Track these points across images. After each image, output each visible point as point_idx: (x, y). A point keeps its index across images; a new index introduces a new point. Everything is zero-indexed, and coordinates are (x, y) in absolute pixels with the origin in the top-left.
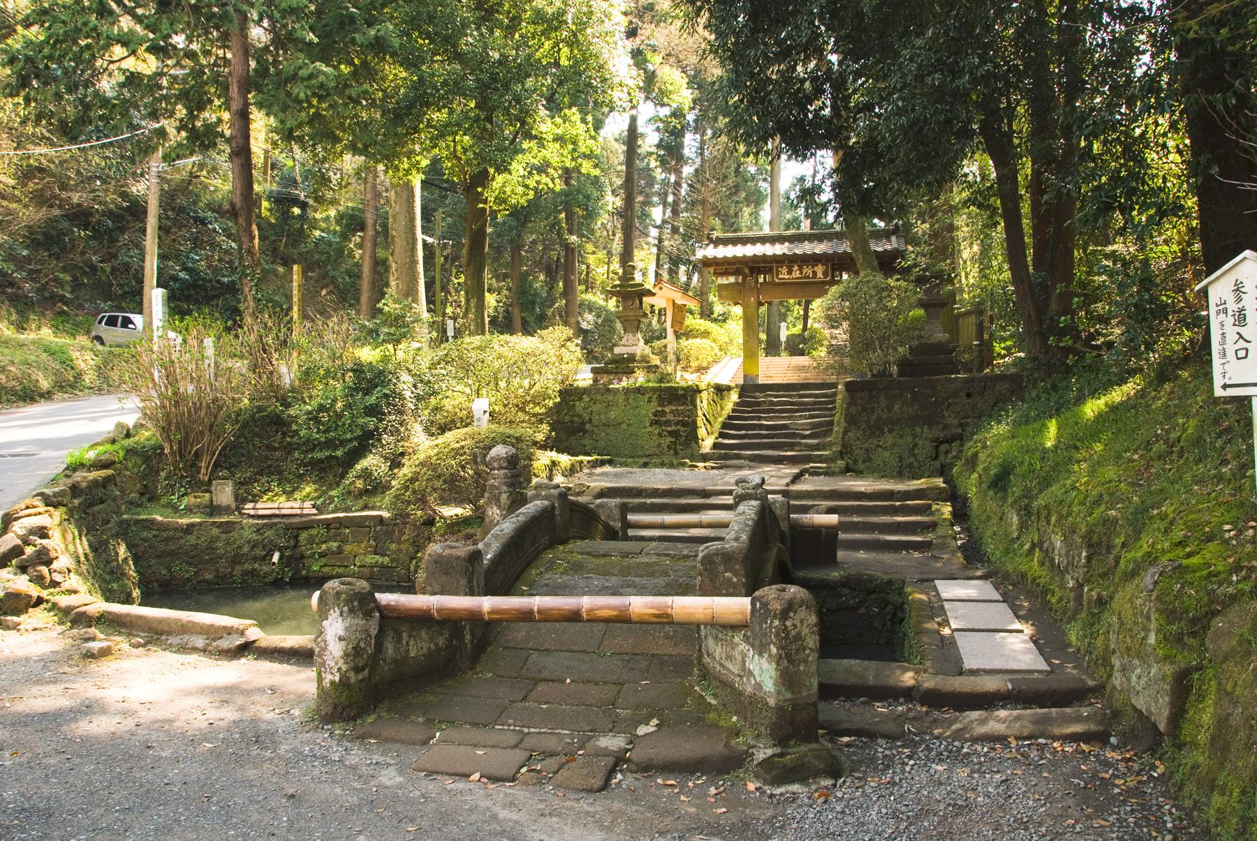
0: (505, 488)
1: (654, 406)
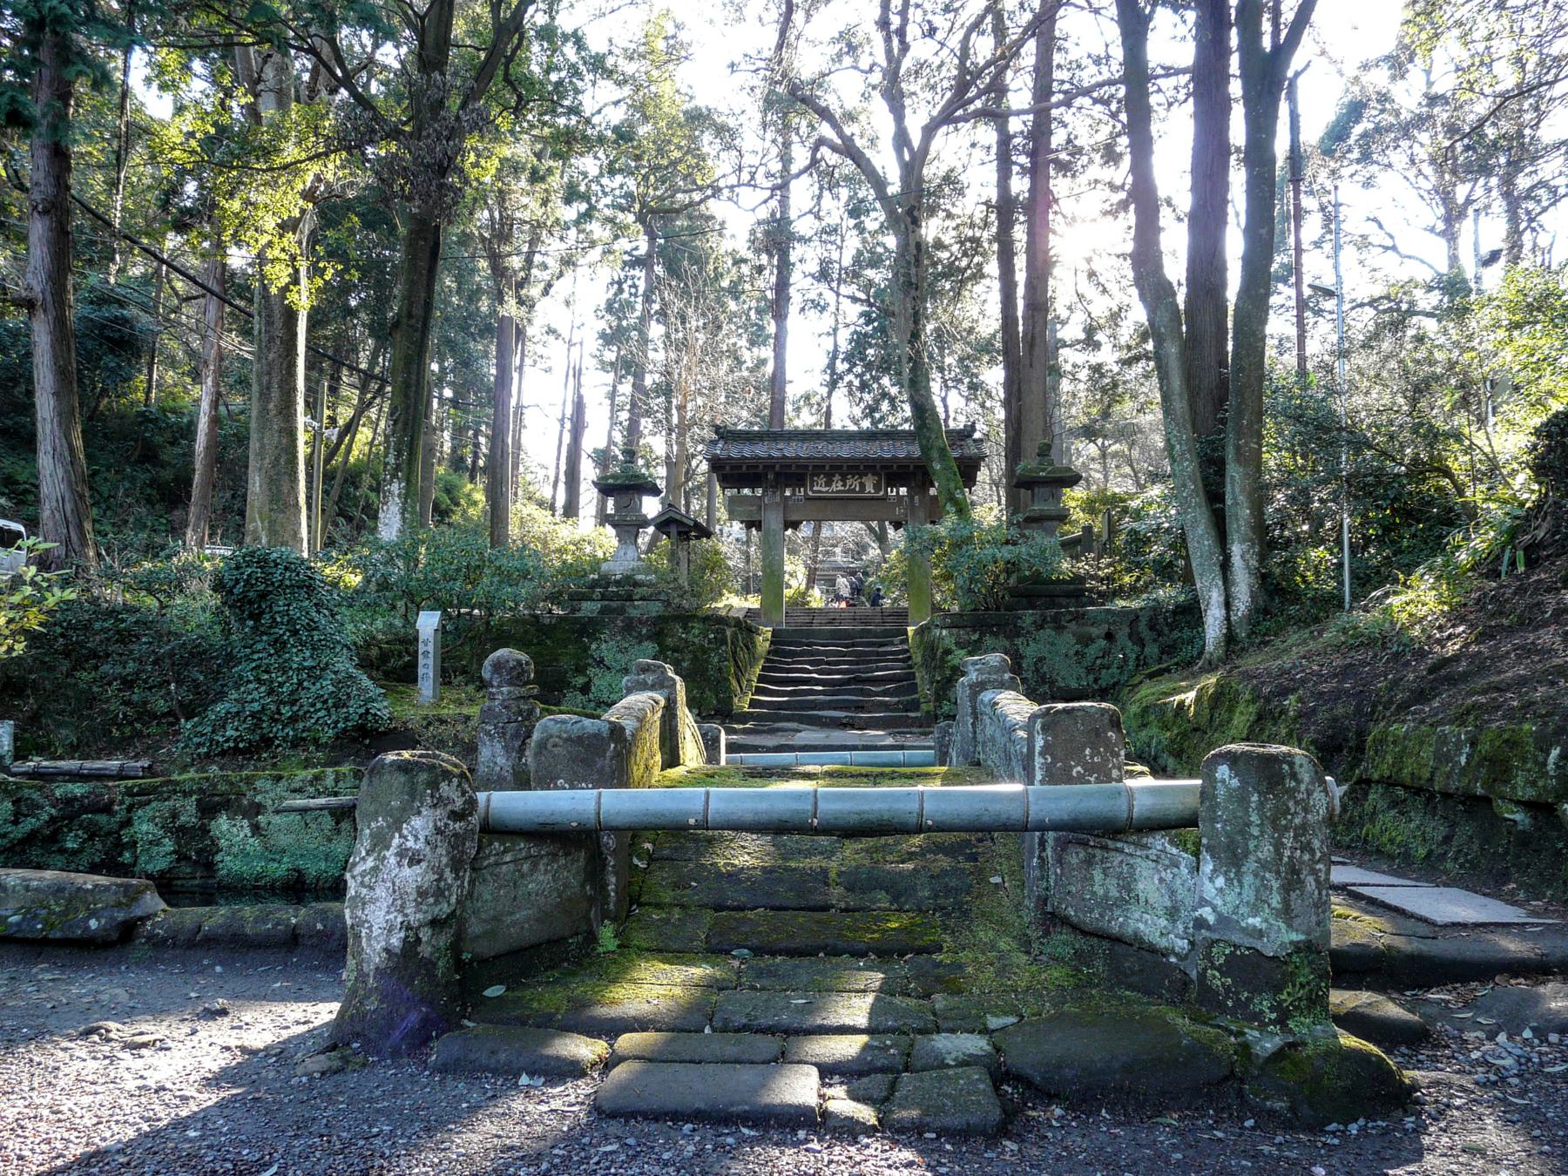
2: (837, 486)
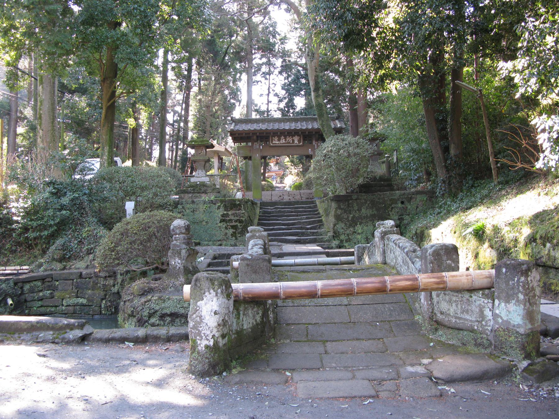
0: (184, 246)
1: (222, 211)
2: (283, 141)
